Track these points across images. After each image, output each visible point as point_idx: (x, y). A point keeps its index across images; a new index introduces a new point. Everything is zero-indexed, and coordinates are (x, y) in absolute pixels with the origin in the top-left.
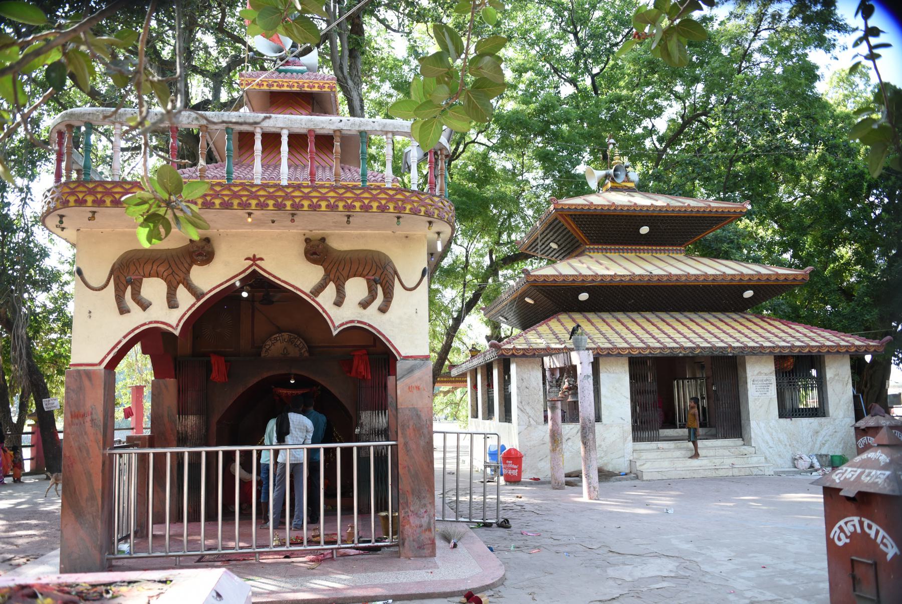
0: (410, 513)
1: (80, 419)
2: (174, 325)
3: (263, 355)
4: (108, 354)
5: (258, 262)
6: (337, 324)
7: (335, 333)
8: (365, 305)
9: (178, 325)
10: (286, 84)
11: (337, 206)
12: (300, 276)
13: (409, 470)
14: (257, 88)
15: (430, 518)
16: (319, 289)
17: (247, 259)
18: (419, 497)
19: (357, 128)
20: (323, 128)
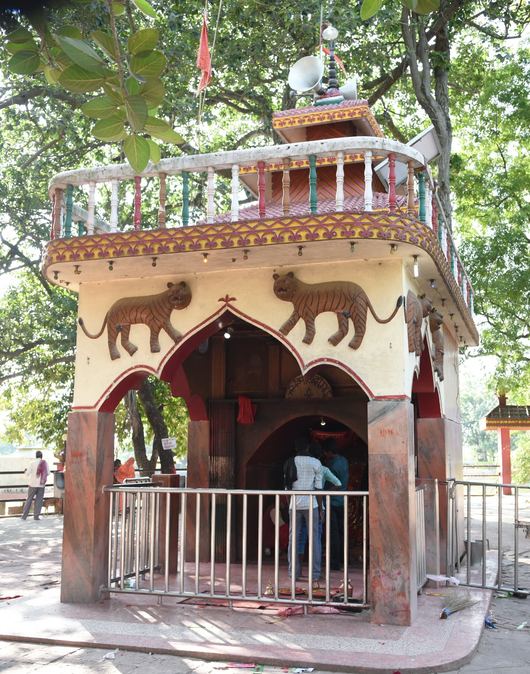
0: (381, 574)
1: (79, 457)
2: (156, 369)
3: (287, 396)
4: (102, 397)
5: (231, 303)
6: (306, 363)
7: (304, 373)
8: (335, 341)
9: (159, 369)
10: (316, 117)
11: (283, 238)
12: (269, 313)
13: (381, 525)
14: (290, 126)
15: (404, 581)
17: (221, 300)
18: (391, 556)
19: (305, 153)
20: (271, 158)
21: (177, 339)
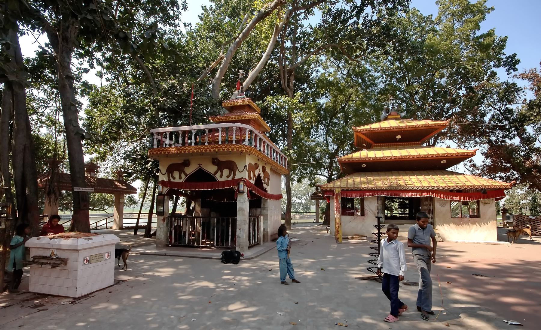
12: (211, 169)
16: (216, 173)
21: (186, 175)
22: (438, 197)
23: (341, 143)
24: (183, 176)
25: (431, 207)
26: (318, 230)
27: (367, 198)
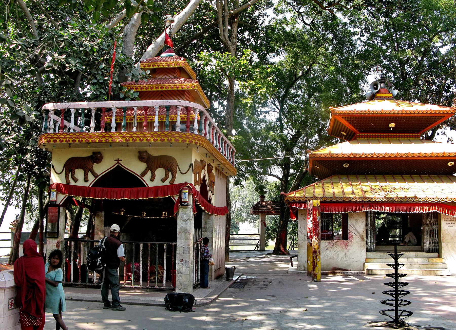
12: (136, 167)
16: (144, 174)
22: (444, 214)
23: (301, 126)
24: (91, 177)
25: (436, 227)
26: (271, 262)
27: (352, 215)
